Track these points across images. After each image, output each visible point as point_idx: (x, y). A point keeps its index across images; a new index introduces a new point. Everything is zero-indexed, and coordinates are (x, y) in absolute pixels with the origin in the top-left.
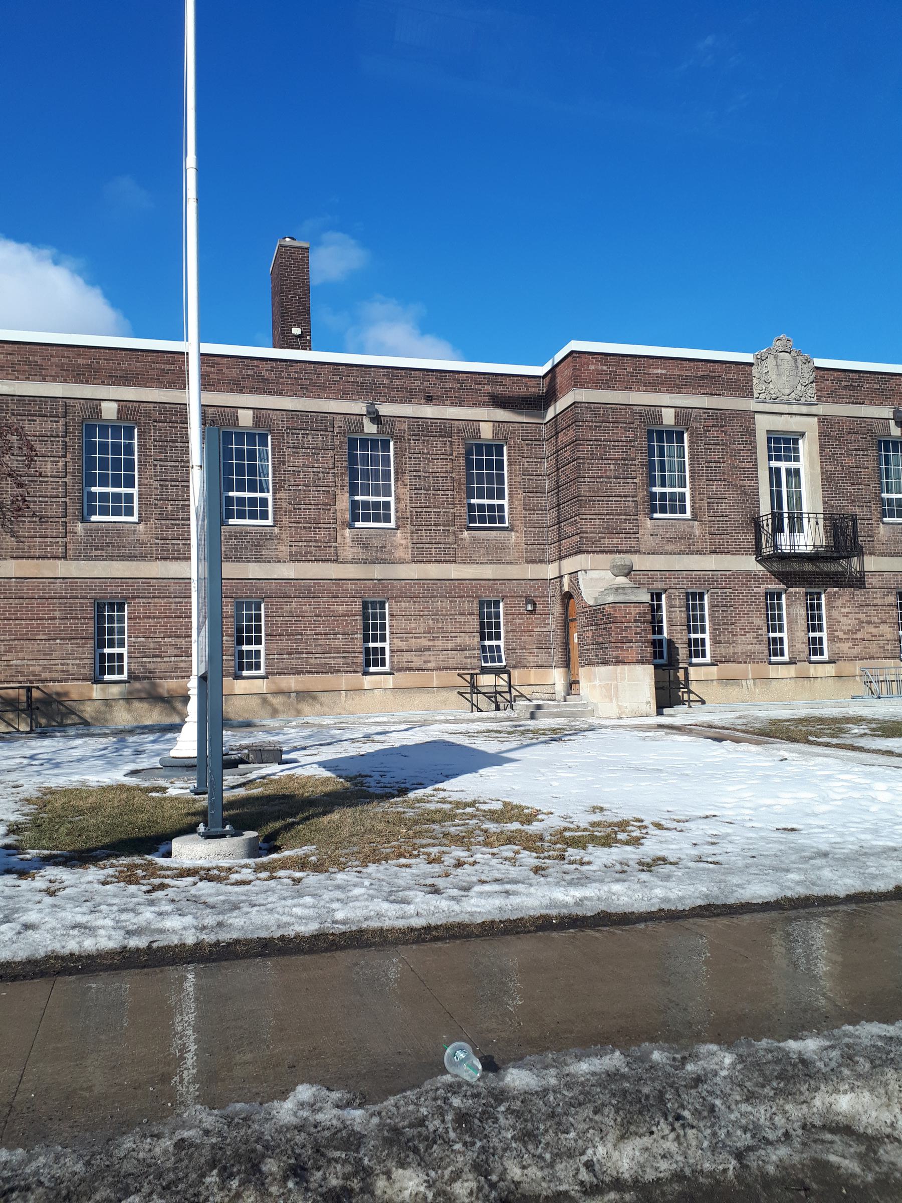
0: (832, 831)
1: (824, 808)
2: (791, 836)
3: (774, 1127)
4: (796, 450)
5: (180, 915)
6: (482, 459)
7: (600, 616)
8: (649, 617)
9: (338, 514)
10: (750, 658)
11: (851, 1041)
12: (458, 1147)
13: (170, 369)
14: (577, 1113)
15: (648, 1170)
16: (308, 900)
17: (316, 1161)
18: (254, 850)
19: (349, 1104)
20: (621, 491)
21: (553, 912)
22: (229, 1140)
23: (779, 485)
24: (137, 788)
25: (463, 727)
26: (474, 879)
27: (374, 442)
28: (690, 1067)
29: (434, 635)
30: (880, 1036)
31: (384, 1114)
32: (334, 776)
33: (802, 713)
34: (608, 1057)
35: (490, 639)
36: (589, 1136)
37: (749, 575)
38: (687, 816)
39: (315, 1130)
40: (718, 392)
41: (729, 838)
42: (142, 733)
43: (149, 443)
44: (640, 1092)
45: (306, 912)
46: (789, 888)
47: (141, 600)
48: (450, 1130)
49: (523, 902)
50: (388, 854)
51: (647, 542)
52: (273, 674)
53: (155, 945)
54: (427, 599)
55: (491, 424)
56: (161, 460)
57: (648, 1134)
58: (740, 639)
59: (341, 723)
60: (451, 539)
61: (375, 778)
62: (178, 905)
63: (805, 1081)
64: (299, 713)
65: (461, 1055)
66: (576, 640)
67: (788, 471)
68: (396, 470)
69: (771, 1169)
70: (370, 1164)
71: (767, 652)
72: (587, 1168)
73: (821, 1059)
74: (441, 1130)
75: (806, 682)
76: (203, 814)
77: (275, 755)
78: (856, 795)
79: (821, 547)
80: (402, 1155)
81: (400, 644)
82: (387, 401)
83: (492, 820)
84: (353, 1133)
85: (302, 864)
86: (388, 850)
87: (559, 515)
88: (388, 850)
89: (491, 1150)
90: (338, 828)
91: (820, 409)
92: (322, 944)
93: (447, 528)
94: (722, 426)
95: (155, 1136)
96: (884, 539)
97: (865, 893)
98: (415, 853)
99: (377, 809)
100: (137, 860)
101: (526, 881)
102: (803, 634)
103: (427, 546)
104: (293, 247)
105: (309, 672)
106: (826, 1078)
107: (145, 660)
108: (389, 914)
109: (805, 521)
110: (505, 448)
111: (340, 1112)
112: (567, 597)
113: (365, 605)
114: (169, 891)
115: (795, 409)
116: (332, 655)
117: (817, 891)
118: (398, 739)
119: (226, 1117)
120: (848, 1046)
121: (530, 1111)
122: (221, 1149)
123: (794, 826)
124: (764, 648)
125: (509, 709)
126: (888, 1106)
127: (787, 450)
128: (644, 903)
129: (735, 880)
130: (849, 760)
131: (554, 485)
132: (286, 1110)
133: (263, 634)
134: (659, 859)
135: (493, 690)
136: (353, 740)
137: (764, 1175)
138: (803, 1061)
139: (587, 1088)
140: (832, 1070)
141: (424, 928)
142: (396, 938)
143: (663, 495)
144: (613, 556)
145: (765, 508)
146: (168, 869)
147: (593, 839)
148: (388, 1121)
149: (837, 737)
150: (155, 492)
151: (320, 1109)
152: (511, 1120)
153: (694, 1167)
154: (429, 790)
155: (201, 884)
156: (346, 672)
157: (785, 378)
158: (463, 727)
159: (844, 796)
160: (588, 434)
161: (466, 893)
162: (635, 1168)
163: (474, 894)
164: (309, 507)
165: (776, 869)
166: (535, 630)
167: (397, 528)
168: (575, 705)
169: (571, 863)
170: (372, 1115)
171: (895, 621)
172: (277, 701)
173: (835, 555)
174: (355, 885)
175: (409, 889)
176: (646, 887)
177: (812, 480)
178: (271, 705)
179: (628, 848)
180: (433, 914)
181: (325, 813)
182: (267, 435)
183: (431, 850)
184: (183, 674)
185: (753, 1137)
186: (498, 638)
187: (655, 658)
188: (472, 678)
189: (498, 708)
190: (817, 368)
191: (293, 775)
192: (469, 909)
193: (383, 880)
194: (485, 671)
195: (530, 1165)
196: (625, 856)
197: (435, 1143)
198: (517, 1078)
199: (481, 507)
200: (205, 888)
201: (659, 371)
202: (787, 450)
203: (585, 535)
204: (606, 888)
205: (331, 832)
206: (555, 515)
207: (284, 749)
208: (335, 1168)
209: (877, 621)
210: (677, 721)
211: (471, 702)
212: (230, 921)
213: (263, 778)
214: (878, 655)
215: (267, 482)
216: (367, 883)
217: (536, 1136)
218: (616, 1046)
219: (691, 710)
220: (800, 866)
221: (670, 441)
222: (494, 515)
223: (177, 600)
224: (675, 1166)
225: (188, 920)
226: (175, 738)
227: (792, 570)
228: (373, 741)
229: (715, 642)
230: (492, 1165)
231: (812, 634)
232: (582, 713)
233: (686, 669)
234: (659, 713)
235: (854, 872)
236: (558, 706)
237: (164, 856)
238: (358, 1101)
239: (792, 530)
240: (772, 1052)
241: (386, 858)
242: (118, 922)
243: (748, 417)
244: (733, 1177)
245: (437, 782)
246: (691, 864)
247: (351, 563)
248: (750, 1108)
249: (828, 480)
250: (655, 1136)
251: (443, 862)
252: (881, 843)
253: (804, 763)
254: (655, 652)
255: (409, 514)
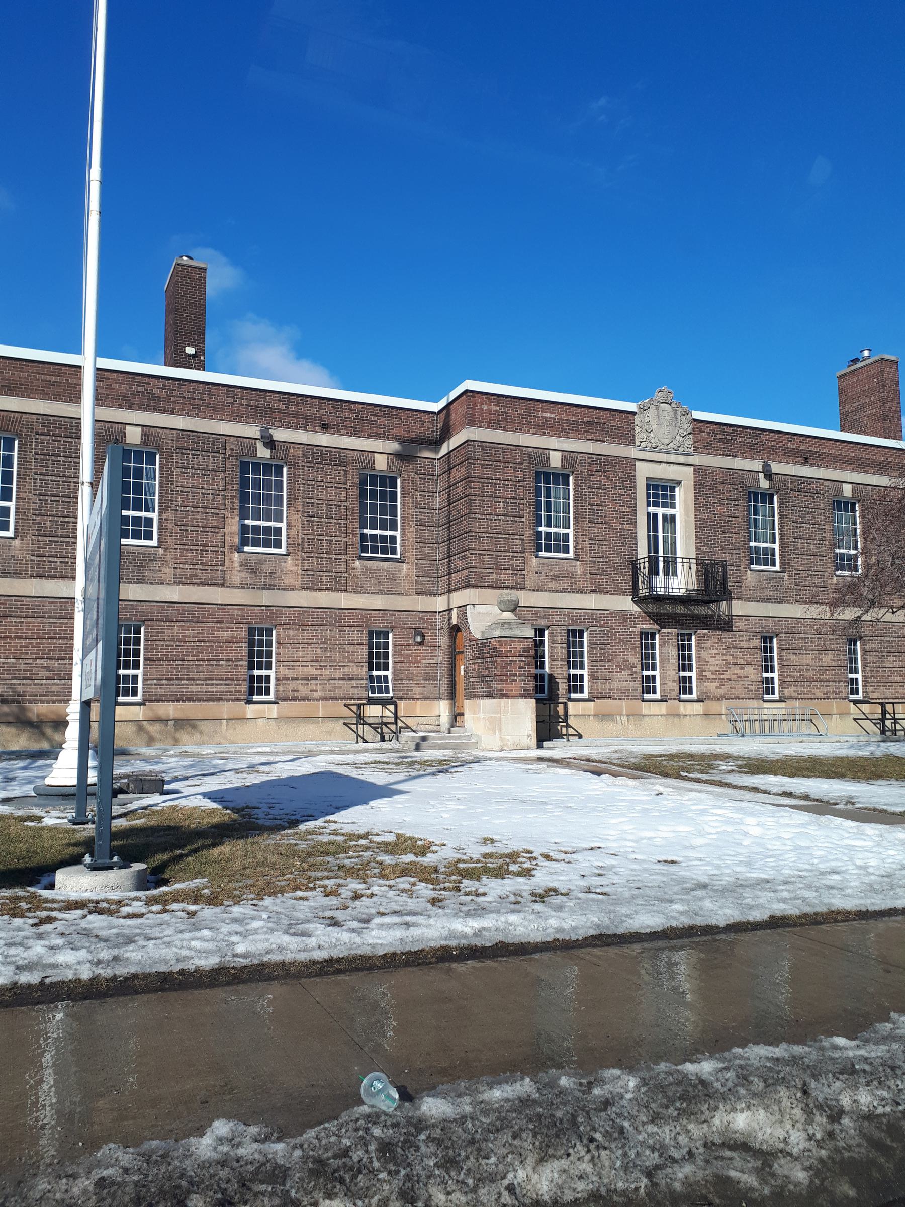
0: (709, 864)
1: (700, 841)
2: (673, 868)
3: (678, 1146)
4: (673, 497)
5: (72, 949)
6: (375, 490)
7: (486, 649)
8: (533, 652)
9: (227, 537)
10: (625, 695)
11: (742, 1062)
12: (383, 1176)
13: (64, 382)
14: (496, 1139)
15: (566, 1191)
16: (206, 933)
17: (242, 1195)
18: (142, 883)
19: (267, 1139)
20: (508, 528)
21: (453, 943)
22: (150, 1178)
23: (656, 530)
24: (10, 817)
25: (350, 758)
26: (373, 911)
27: (267, 467)
28: (597, 1091)
29: (322, 664)
30: (767, 1058)
31: (306, 1146)
32: (220, 807)
33: (673, 749)
34: (518, 1084)
35: (378, 669)
36: (509, 1160)
37: (626, 615)
38: (573, 848)
39: (237, 1165)
40: (602, 438)
41: (614, 870)
42: (10, 760)
43: (30, 455)
44: (554, 1116)
45: (205, 945)
46: (674, 918)
47: (14, 619)
48: (374, 1159)
49: (423, 934)
50: (284, 886)
51: (532, 579)
52: (151, 701)
53: (48, 981)
54: (316, 628)
55: (386, 456)
56: (41, 474)
57: (565, 1156)
58: (616, 676)
59: (221, 753)
60: (343, 568)
61: (263, 809)
62: (69, 938)
63: (705, 1102)
64: (176, 742)
65: (379, 1086)
66: (462, 673)
67: (665, 517)
68: (289, 496)
69: (677, 1186)
70: (297, 1196)
71: (640, 689)
72: (510, 1191)
73: (718, 1080)
74: (364, 1160)
75: (676, 719)
76: (88, 845)
77: (157, 785)
78: (730, 829)
79: (694, 590)
80: (329, 1186)
81: (286, 672)
82: (282, 426)
83: (386, 852)
84: (277, 1166)
85: (195, 897)
86: (283, 883)
87: (449, 550)
88: (283, 883)
89: (416, 1178)
90: (229, 860)
91: (696, 460)
92: (223, 978)
93: (339, 557)
94: (605, 471)
95: (70, 1176)
96: (751, 585)
97: (743, 923)
98: (311, 885)
99: (268, 841)
100: (20, 892)
101: (425, 913)
102: (674, 673)
103: (318, 573)
104: (191, 266)
105: (189, 700)
106: (724, 1098)
107: (14, 682)
108: (291, 947)
109: (679, 565)
110: (399, 481)
111: (261, 1146)
112: (455, 630)
113: (251, 631)
114: (57, 924)
115: (673, 458)
116: (214, 682)
117: (699, 921)
118: (284, 770)
119: (143, 1155)
120: (741, 1067)
121: (450, 1139)
122: (144, 1186)
123: (674, 859)
124: (637, 685)
125: (394, 741)
126: (781, 1122)
127: (665, 496)
128: (539, 933)
129: (624, 910)
130: (719, 795)
131: (445, 520)
132: (205, 1146)
133: (142, 659)
134: (550, 890)
135: (379, 721)
136: (237, 771)
137: (672, 1192)
138: (703, 1082)
139: (503, 1114)
140: (729, 1090)
141: (326, 961)
142: (299, 971)
143: (548, 534)
144: (500, 591)
145: (642, 551)
146: (53, 901)
147: (486, 871)
148: (311, 1153)
149: (707, 773)
150: (33, 506)
151: (239, 1145)
152: (433, 1148)
153: (609, 1187)
154: (320, 822)
155: (90, 917)
156: (228, 700)
157: (665, 428)
158: (350, 758)
159: (719, 830)
160: (480, 472)
161: (366, 926)
162: (554, 1190)
163: (374, 926)
164: (197, 529)
165: (661, 900)
166: (423, 661)
167: (288, 554)
168: (459, 737)
169: (467, 894)
170: (294, 1147)
171: (759, 663)
172: (154, 729)
173: (706, 598)
174: (253, 919)
175: (308, 921)
176: (541, 917)
177: (686, 527)
178: (148, 733)
179: (521, 880)
180: (335, 947)
181: (214, 845)
182: (155, 454)
183: (327, 882)
184: (55, 698)
185: (660, 1156)
186: (386, 668)
187: (537, 692)
188: (359, 708)
189: (383, 739)
190: (695, 420)
191: (177, 806)
192: (371, 942)
193: (281, 913)
194: (371, 701)
195: (454, 1191)
196: (518, 887)
197: (360, 1172)
198: (433, 1107)
199: (374, 537)
200: (96, 921)
201: (548, 415)
202: (665, 496)
203: (474, 570)
204: (503, 919)
205: (222, 864)
206: (445, 549)
207: (166, 779)
208: (262, 1201)
209: (742, 662)
210: (557, 754)
211: (357, 733)
212: (127, 955)
213: (145, 808)
214: (743, 696)
215: (153, 501)
216: (265, 916)
217: (458, 1162)
218: (524, 1074)
219: (569, 744)
220: (683, 897)
221: (556, 483)
222: (386, 545)
223: (51, 620)
224: (591, 1186)
225: (83, 954)
226: (51, 766)
227: (666, 612)
228: (258, 772)
229: (593, 678)
230: (417, 1193)
231: (682, 674)
232: (467, 745)
233: (565, 704)
234: (540, 746)
235: (732, 903)
236: (442, 738)
237: (46, 888)
238: (275, 1135)
239: (666, 574)
240: (672, 1074)
241: (282, 891)
242: (6, 957)
243: (629, 464)
244: (644, 1195)
245: (327, 814)
246: (581, 895)
247: (239, 588)
248: (655, 1129)
249: (701, 526)
250: (571, 1158)
251: (340, 894)
252: (754, 875)
253: (678, 797)
254: (537, 686)
255: (300, 541)
